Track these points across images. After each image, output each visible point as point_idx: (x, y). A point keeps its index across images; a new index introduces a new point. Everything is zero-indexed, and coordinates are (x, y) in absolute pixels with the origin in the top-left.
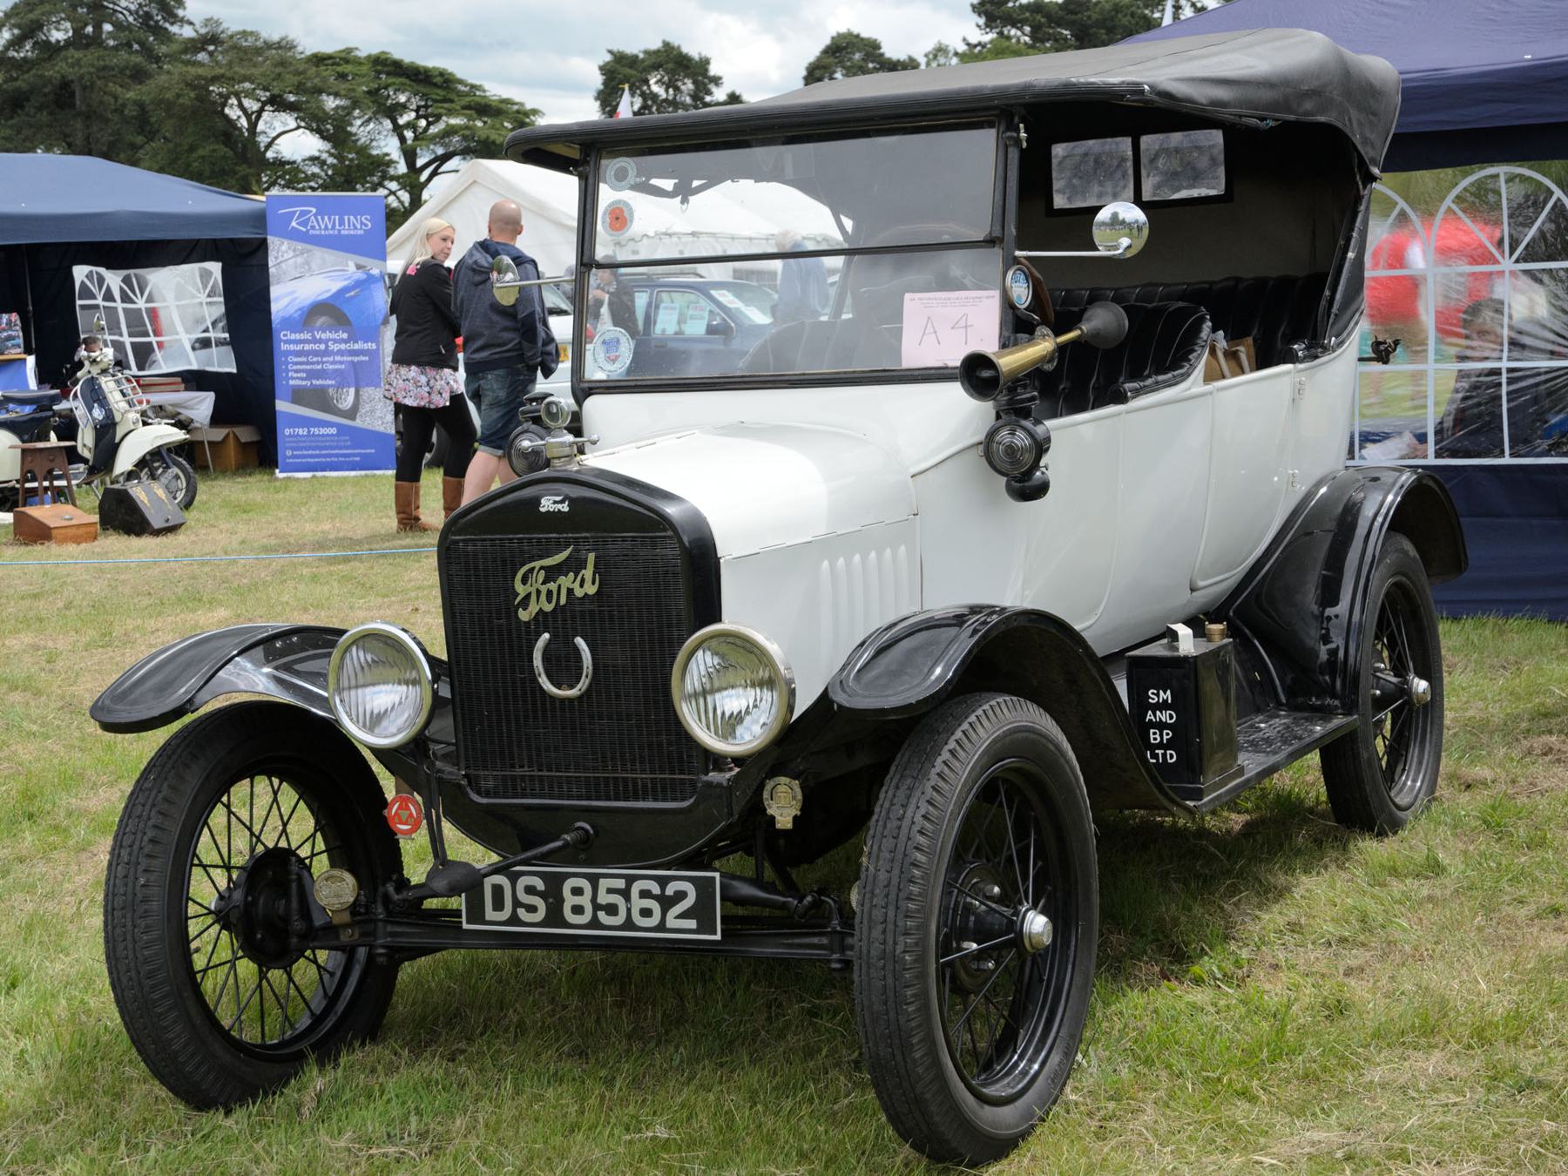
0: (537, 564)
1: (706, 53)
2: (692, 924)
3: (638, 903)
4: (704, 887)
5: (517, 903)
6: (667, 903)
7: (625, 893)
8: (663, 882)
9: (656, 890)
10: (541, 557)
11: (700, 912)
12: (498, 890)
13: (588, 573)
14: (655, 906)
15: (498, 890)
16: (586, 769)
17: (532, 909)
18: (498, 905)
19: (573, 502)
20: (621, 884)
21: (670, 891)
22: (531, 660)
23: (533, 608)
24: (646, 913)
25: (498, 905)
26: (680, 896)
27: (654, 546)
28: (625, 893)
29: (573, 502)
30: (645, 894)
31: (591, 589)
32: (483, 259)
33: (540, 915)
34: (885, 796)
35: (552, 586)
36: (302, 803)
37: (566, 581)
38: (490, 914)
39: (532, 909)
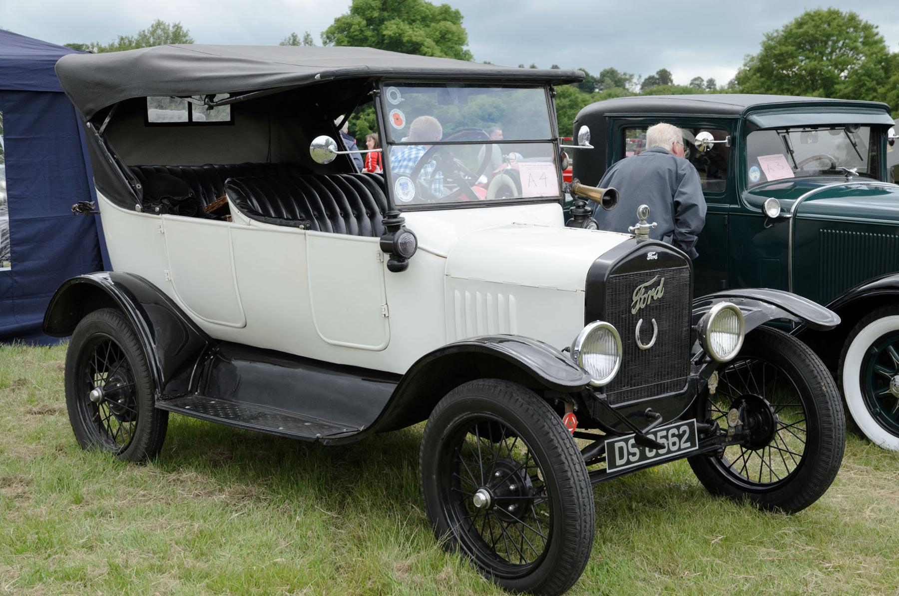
0: (643, 286)
1: (829, 6)
2: (688, 444)
3: (672, 440)
4: (691, 425)
5: (629, 453)
6: (680, 437)
7: (666, 437)
8: (678, 427)
9: (677, 433)
10: (644, 282)
11: (691, 439)
12: (621, 449)
13: (660, 288)
14: (676, 439)
15: (621, 449)
16: (648, 382)
17: (634, 454)
18: (621, 457)
19: (659, 254)
20: (664, 433)
21: (681, 432)
22: (659, 331)
23: (637, 307)
24: (674, 444)
25: (621, 457)
26: (684, 432)
27: (680, 273)
28: (666, 437)
29: (659, 254)
30: (673, 435)
31: (660, 295)
32: (406, 191)
33: (637, 458)
34: (106, 310)
35: (646, 296)
36: (389, 388)
37: (651, 293)
38: (619, 462)
39: (634, 454)
